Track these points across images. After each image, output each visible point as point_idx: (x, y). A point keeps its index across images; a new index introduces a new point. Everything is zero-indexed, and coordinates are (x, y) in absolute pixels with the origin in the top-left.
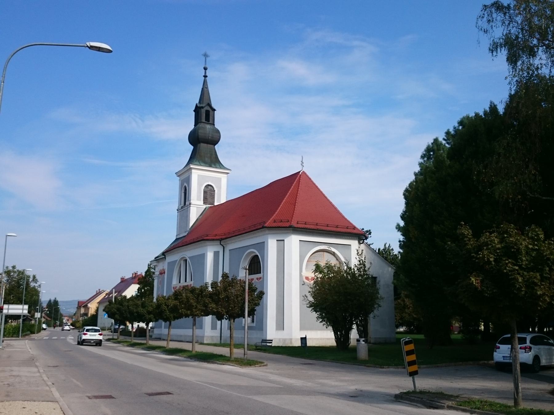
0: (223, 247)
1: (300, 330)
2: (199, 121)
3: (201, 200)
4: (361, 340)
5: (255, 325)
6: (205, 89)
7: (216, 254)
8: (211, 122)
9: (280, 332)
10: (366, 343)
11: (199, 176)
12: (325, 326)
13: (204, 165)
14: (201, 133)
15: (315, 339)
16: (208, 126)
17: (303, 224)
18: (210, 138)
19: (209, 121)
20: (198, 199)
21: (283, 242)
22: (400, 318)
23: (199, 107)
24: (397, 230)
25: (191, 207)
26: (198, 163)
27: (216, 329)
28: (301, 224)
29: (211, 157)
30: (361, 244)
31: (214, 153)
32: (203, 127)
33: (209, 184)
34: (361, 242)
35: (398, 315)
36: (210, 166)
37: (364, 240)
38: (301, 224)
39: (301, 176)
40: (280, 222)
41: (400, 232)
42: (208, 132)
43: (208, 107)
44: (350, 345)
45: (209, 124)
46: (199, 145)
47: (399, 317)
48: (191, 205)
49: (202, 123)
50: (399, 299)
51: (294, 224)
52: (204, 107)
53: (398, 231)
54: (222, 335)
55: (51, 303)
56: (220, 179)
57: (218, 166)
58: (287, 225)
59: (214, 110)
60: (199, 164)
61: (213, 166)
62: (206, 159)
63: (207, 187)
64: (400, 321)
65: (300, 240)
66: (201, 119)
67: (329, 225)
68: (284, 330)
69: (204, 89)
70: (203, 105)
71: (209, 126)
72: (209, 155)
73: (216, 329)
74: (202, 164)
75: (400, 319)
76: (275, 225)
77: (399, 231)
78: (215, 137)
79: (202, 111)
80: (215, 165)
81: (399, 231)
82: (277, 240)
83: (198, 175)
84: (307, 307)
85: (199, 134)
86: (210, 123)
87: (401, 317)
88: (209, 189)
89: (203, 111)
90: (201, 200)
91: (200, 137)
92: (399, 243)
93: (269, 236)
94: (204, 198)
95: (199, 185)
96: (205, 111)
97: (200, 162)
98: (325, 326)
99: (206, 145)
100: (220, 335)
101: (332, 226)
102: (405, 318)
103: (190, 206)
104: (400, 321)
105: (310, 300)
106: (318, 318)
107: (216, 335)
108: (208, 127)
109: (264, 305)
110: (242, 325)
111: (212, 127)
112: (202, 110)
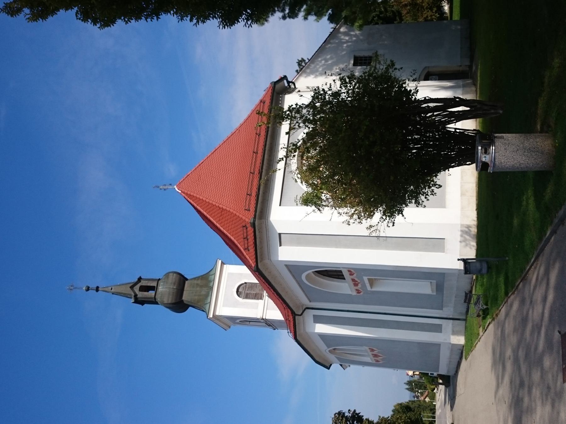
0: (307, 310)
1: (444, 207)
2: (154, 301)
3: (258, 303)
4: (484, 160)
5: (435, 281)
6: (113, 291)
7: (318, 320)
8: (154, 284)
9: (448, 245)
10: (492, 142)
11: (224, 305)
12: (436, 190)
13: (209, 298)
14: (168, 299)
15: (462, 177)
16: (160, 289)
17: (250, 200)
18: (175, 287)
19: (154, 287)
20: (257, 307)
21: (282, 235)
22: (430, 11)
23: (135, 300)
24: (266, 23)
25: (266, 318)
26: (208, 306)
27: (441, 325)
28: (249, 204)
29: (201, 286)
30: (297, 87)
31: (196, 282)
32: (161, 297)
33: (236, 290)
34: (293, 86)
35: (425, 14)
36: (211, 288)
37: (289, 82)
38: (249, 204)
39: (183, 190)
40: (248, 240)
41: (269, 17)
42: (167, 290)
43: (135, 287)
44: (481, 130)
45: (158, 288)
46: (185, 302)
47: (428, 12)
48: (264, 318)
49: (156, 297)
50: (400, 14)
51: (249, 218)
52: (135, 293)
53: (267, 21)
54: (451, 317)
55: (410, 388)
56: (230, 275)
57: (213, 277)
58: (250, 230)
59: (140, 279)
60: (208, 305)
61: (211, 284)
62: (203, 293)
63: (240, 294)
64: (434, 11)
65: (280, 205)
66: (151, 298)
67: (255, 151)
68: (444, 239)
69: (112, 292)
70: (133, 294)
71: (160, 288)
72: (198, 289)
73: (441, 325)
74: (209, 301)
75: (432, 11)
76: (252, 250)
77: (267, 19)
78: (174, 280)
79: (141, 296)
80: (210, 281)
81: (267, 19)
82: (280, 245)
83: (223, 306)
84: (393, 225)
85: (170, 302)
86: (156, 286)
87: (428, 10)
88: (243, 290)
89: (141, 295)
90: (258, 303)
91: (173, 302)
92: (288, 19)
93: (273, 258)
94: (255, 299)
95: (235, 305)
96: (141, 292)
97: (206, 303)
98: (436, 190)
99: (185, 293)
100: (452, 321)
101: (256, 141)
102: (429, 4)
103: (266, 319)
104: (434, 11)
105: (378, 220)
106: (418, 204)
107: (450, 325)
108: (161, 290)
109: (397, 270)
110: (434, 295)
111: (161, 283)
112: (138, 296)
